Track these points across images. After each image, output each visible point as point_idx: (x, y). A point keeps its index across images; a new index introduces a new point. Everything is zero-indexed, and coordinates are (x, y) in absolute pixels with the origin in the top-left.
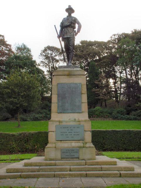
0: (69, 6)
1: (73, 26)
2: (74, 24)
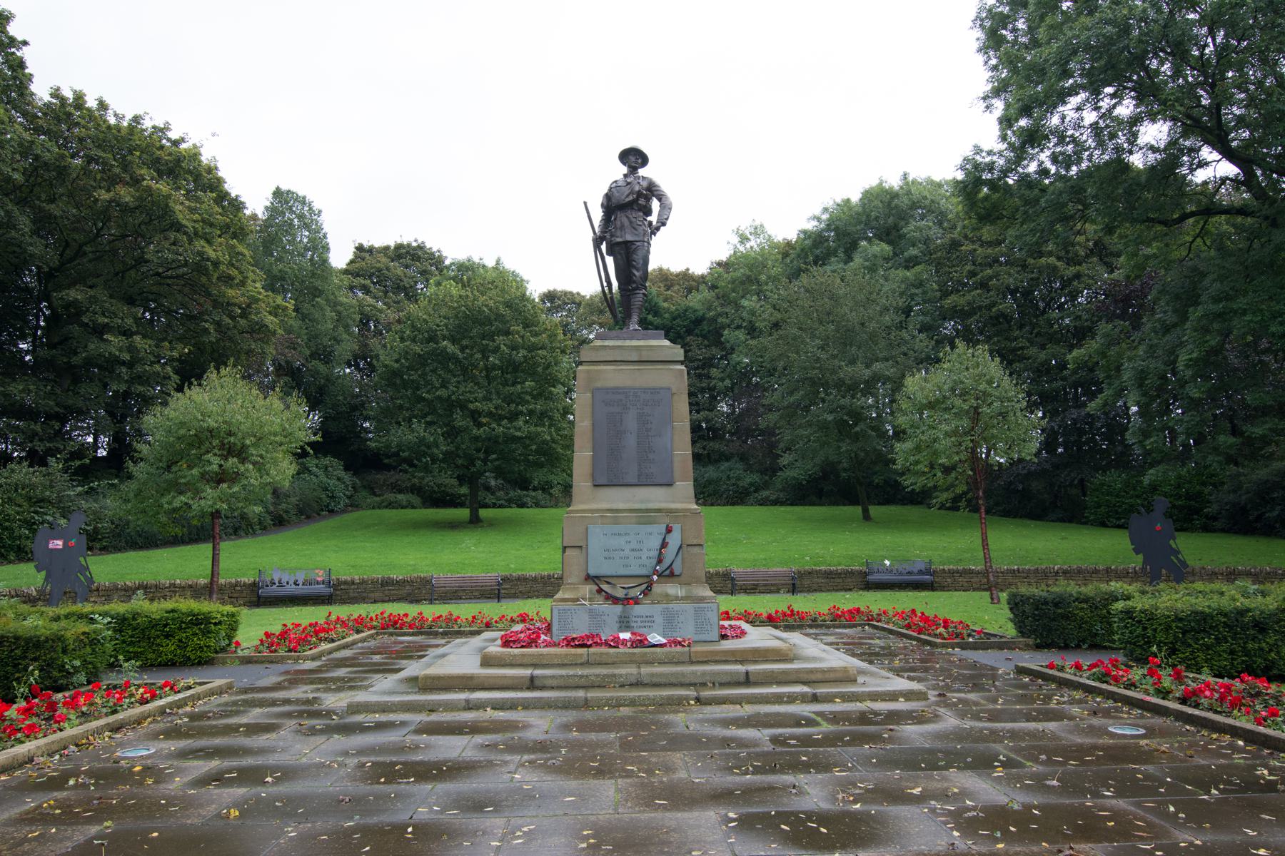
1: (645, 207)
2: (648, 199)
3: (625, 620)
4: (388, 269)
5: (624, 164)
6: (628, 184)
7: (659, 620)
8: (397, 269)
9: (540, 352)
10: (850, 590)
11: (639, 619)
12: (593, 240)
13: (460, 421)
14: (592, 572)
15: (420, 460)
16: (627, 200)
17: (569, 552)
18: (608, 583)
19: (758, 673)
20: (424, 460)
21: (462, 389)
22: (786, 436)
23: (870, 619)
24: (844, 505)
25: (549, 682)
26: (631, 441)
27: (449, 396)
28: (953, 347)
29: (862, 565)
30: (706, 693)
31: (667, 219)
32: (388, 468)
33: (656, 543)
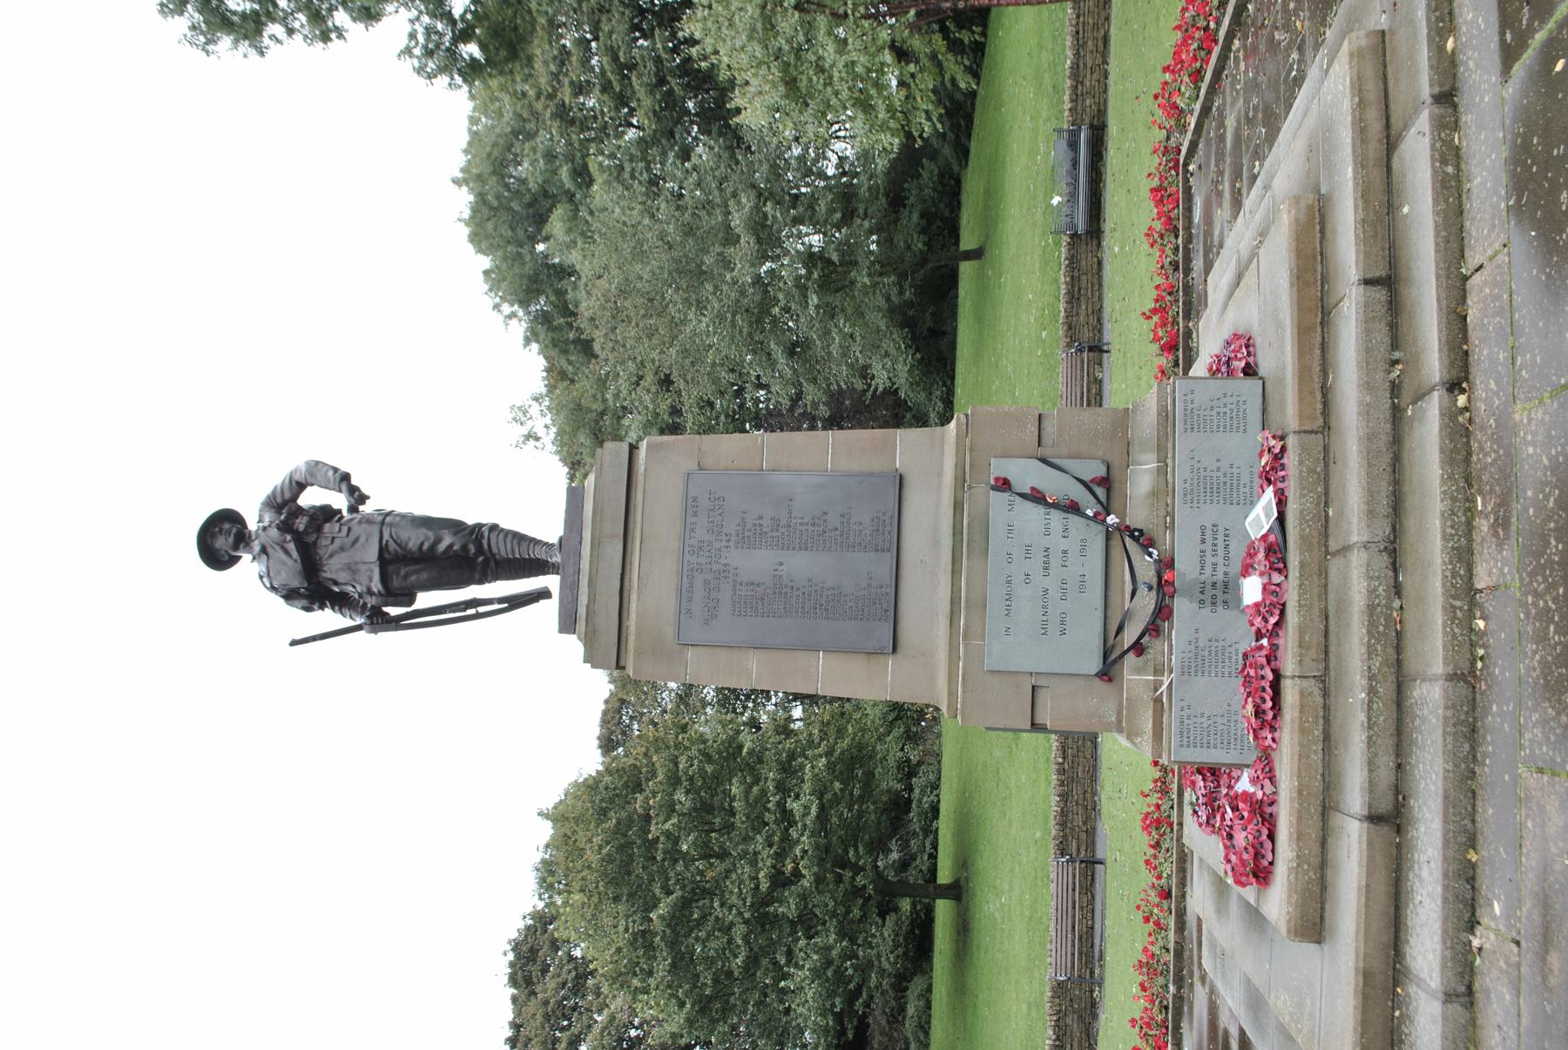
0: (368, 498)
2: (300, 511)
3: (1209, 592)
4: (546, 1003)
5: (234, 560)
6: (264, 550)
7: (1211, 514)
8: (548, 987)
9: (681, 766)
10: (1100, 263)
11: (1209, 560)
12: (375, 631)
13: (788, 907)
14: (1094, 664)
15: (851, 978)
16: (295, 554)
17: (1044, 718)
18: (1120, 629)
19: (1366, 256)
20: (850, 972)
21: (734, 900)
22: (841, 375)
23: (1175, 161)
24: (956, 296)
25: (1385, 775)
26: (800, 565)
27: (746, 922)
28: (691, 41)
29: (1057, 244)
30: (1433, 363)
31: (336, 470)
32: (862, 1027)
33: (1034, 512)
